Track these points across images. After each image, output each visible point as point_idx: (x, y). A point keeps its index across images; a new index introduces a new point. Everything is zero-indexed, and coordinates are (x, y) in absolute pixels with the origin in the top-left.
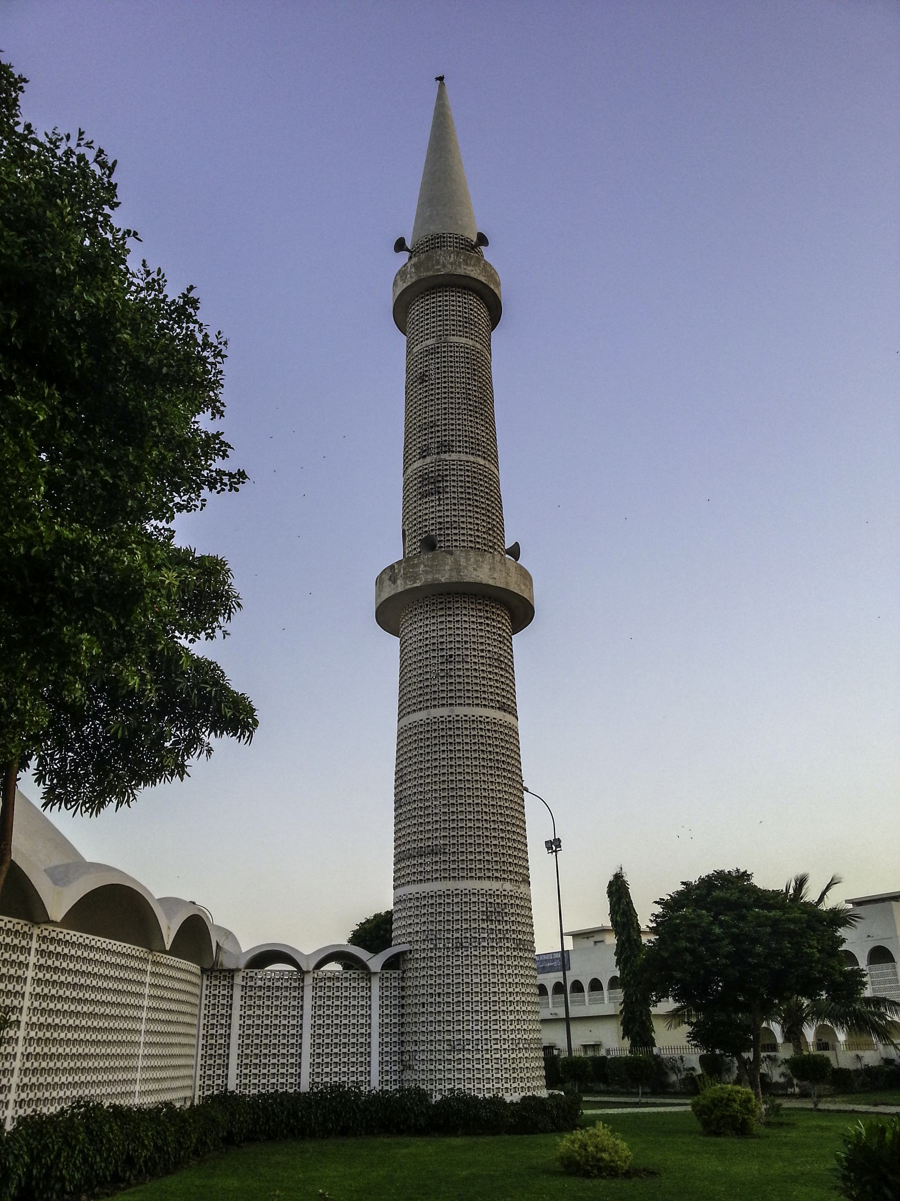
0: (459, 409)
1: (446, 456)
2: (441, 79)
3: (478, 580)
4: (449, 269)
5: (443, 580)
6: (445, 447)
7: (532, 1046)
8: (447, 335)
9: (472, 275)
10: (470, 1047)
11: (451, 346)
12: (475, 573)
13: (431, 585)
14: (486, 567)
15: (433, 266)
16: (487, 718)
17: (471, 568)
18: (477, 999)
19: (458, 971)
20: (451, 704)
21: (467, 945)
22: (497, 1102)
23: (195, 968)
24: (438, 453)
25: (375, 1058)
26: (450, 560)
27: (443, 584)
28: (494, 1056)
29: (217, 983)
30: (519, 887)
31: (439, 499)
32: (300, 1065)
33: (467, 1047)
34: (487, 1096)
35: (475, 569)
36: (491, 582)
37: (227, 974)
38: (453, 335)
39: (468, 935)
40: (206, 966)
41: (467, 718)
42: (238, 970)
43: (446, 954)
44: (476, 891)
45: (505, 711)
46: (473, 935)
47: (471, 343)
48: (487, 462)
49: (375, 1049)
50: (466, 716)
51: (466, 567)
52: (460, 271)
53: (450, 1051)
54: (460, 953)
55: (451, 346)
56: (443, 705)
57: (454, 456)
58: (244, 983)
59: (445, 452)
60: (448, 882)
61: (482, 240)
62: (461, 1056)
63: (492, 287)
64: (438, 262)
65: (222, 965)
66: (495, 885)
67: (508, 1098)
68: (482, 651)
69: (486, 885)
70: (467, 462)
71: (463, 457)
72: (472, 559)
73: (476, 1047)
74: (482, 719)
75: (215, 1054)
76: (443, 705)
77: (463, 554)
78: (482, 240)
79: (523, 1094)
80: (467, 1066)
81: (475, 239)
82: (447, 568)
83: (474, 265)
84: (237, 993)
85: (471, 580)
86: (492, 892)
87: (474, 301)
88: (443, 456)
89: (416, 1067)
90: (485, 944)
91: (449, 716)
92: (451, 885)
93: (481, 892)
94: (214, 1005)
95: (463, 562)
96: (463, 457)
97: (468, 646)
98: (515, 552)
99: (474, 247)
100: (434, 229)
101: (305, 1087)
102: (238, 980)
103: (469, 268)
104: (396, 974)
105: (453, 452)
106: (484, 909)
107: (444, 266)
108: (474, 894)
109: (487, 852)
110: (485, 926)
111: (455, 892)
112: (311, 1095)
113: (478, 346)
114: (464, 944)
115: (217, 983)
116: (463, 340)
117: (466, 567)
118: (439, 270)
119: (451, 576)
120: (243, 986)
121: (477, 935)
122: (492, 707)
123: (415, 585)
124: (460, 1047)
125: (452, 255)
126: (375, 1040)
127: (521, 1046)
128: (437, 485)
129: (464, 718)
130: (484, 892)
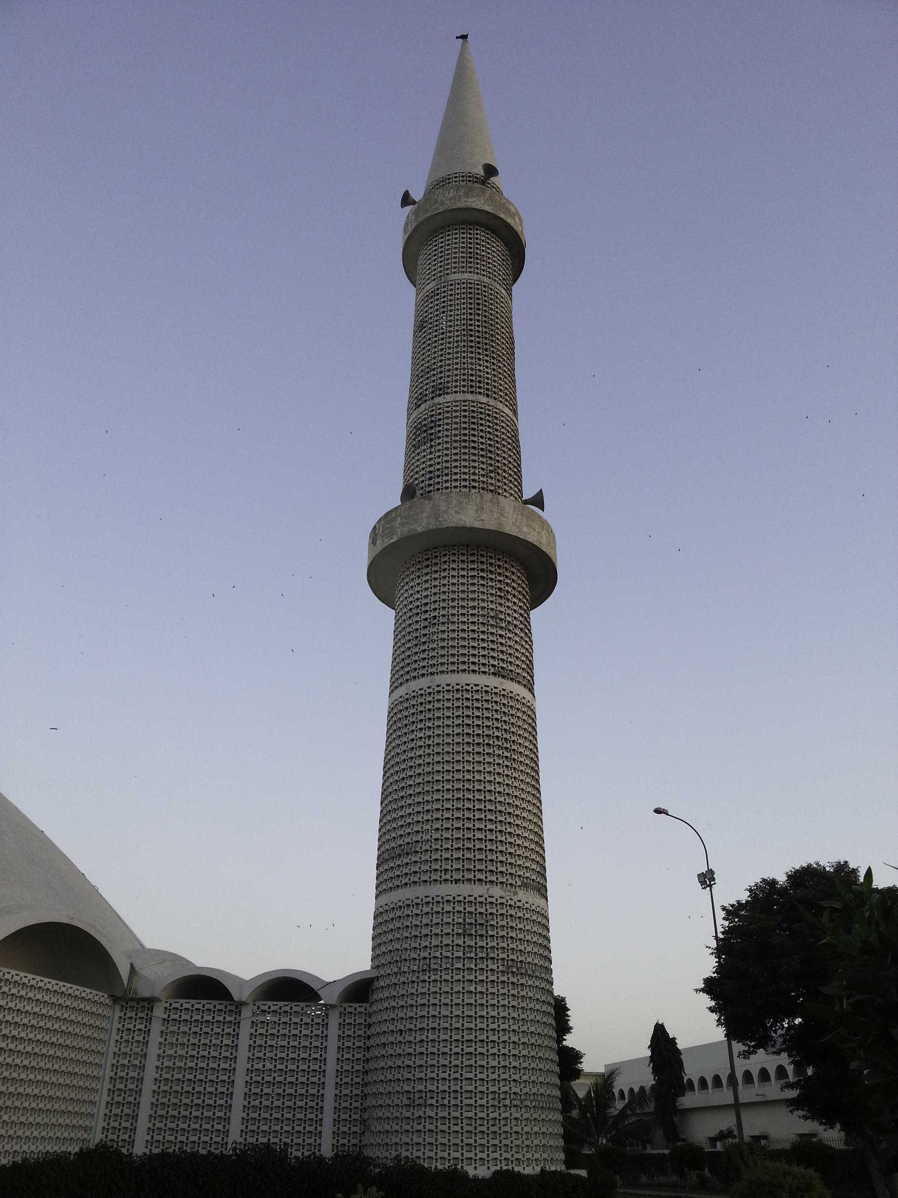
0: (457, 347)
1: (440, 400)
2: (464, 37)
3: (461, 524)
4: (449, 205)
5: (419, 530)
6: (440, 390)
7: (528, 1103)
8: (447, 274)
9: (474, 206)
10: (434, 1102)
11: (451, 285)
12: (457, 516)
13: (408, 537)
14: (471, 510)
15: (431, 206)
16: (476, 685)
17: (452, 512)
18: (457, 1037)
19: (423, 1001)
20: (432, 674)
21: (436, 967)
22: (455, 1177)
23: (102, 997)
24: (433, 398)
25: (328, 1116)
26: (428, 506)
27: (421, 534)
28: (465, 1114)
29: (133, 1015)
30: (516, 893)
31: (431, 446)
32: (228, 1120)
33: (429, 1102)
34: (440, 1167)
35: (457, 512)
36: (477, 525)
37: (145, 1004)
38: (455, 273)
39: (438, 954)
40: (119, 994)
41: (450, 688)
42: (158, 1000)
43: (410, 979)
44: (451, 898)
45: (503, 677)
46: (445, 954)
47: (476, 277)
48: (498, 403)
49: (329, 1104)
50: (448, 685)
51: (446, 512)
52: (459, 205)
53: (409, 1105)
54: (426, 978)
55: (451, 285)
56: (423, 675)
57: (449, 398)
58: (166, 1016)
59: (440, 395)
60: (428, 887)
61: (491, 171)
62: (421, 1113)
63: (502, 216)
64: (436, 202)
65: (135, 992)
66: (478, 890)
67: (471, 1172)
68: (474, 608)
69: (465, 890)
70: (464, 401)
71: (460, 397)
72: (454, 502)
73: (440, 1102)
74: (469, 688)
75: (124, 1101)
76: (423, 675)
77: (443, 497)
78: (491, 171)
79: (493, 1169)
80: (428, 1127)
81: (482, 172)
82: (425, 515)
83: (478, 196)
84: (156, 1027)
85: (451, 525)
86: (472, 899)
87: (481, 235)
88: (437, 400)
89: (373, 1128)
90: (460, 965)
91: (429, 688)
92: (420, 891)
93: (458, 899)
94: (127, 1041)
95: (443, 506)
96: (460, 397)
97: (455, 604)
98: (538, 501)
99: (484, 182)
100: (444, 173)
101: (139, 1149)
102: (159, 1012)
103: (470, 200)
104: (360, 1007)
105: (447, 393)
106: (461, 920)
107: (442, 203)
108: (448, 901)
109: (501, 852)
110: (460, 942)
111: (425, 900)
112: (150, 1158)
113: (486, 280)
114: (432, 966)
115: (133, 1015)
116: (466, 276)
117: (446, 512)
118: (437, 209)
119: (428, 524)
120: (164, 1019)
121: (449, 954)
122: (484, 672)
123: (392, 541)
124: (421, 1101)
125: (451, 191)
126: (330, 1092)
127: (508, 1102)
128: (429, 432)
129: (446, 688)
130: (461, 898)
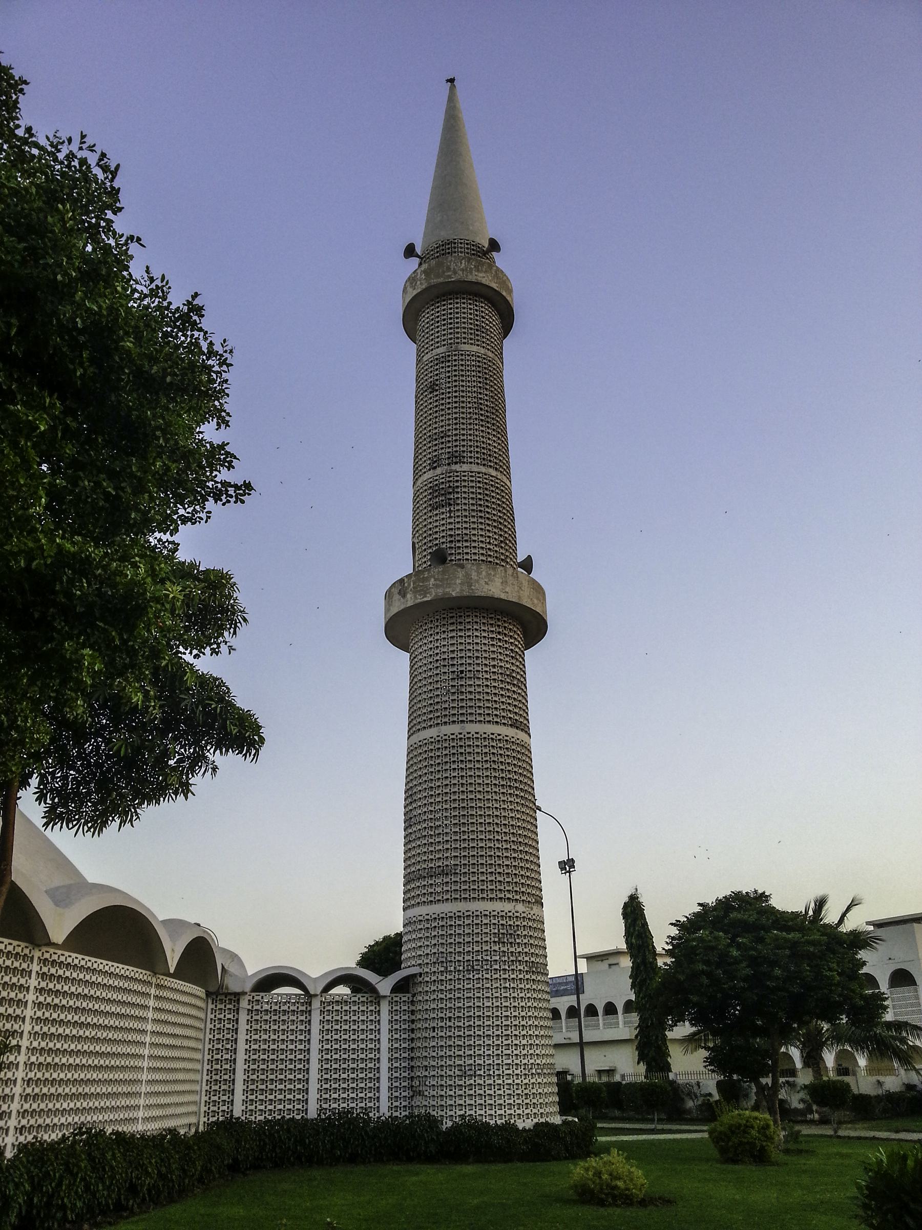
0: (470, 418)
1: (456, 467)
2: (451, 81)
3: (490, 594)
4: (460, 276)
5: (454, 594)
6: (456, 458)
7: (545, 1071)
8: (458, 343)
9: (484, 281)
10: (482, 1072)
11: (462, 355)
12: (486, 586)
13: (442, 599)
14: (498, 581)
15: (444, 272)
16: (499, 735)
17: (482, 582)
18: (488, 1023)
19: (469, 995)
20: (462, 721)
21: (479, 967)
22: (509, 1128)
23: (200, 991)
24: (449, 464)
25: (384, 1084)
26: (461, 573)
27: (454, 598)
28: (506, 1082)
29: (222, 1006)
30: (532, 909)
31: (450, 511)
32: (307, 1091)
33: (478, 1073)
34: (499, 1122)
35: (486, 583)
36: (503, 596)
37: (232, 997)
38: (465, 343)
39: (479, 958)
40: (211, 989)
41: (478, 736)
42: (244, 993)
43: (457, 977)
44: (488, 913)
45: (517, 728)
46: (485, 958)
47: (483, 351)
48: (499, 474)
49: (384, 1075)
50: (477, 733)
51: (477, 581)
52: (471, 278)
53: (461, 1076)
54: (471, 976)
55: (462, 355)
56: (454, 722)
57: (465, 467)
58: (250, 1007)
59: (456, 463)
60: (459, 903)
61: (494, 245)
62: (472, 1082)
63: (504, 294)
64: (449, 269)
65: (227, 988)
66: (507, 907)
67: (520, 1125)
68: (494, 666)
69: (498, 906)
70: (479, 473)
71: (475, 468)
72: (484, 573)
73: (487, 1073)
74: (494, 737)
75: (220, 1079)
76: (454, 722)
77: (475, 568)
78: (494, 245)
79: (536, 1121)
80: (478, 1092)
81: (486, 245)
82: (458, 581)
83: (486, 272)
84: (243, 1017)
85: (483, 594)
86: (504, 914)
87: (485, 309)
88: (454, 467)
89: (426, 1093)
90: (497, 967)
91: (460, 734)
92: (462, 906)
93: (493, 913)
94: (219, 1029)
95: (474, 575)
96: (475, 468)
97: (479, 661)
98: (527, 565)
99: (485, 253)
100: (445, 234)
101: (312, 1114)
102: (244, 1004)
103: (481, 275)
104: (405, 997)
105: (464, 463)
106: (496, 931)
107: (455, 272)
108: (486, 915)
109: (499, 873)
110: (497, 948)
111: (466, 914)
112: (318, 1122)
113: (490, 354)
114: (475, 967)
115: (222, 1006)
116: (475, 348)
117: (477, 581)
118: (450, 277)
119: (462, 590)
120: (249, 1010)
121: (488, 958)
122: (504, 724)
123: (425, 599)
124: (472, 1073)
125: (463, 262)
126: (384, 1065)
127: (534, 1071)
128: (448, 497)
129: (476, 736)
130: (495, 913)
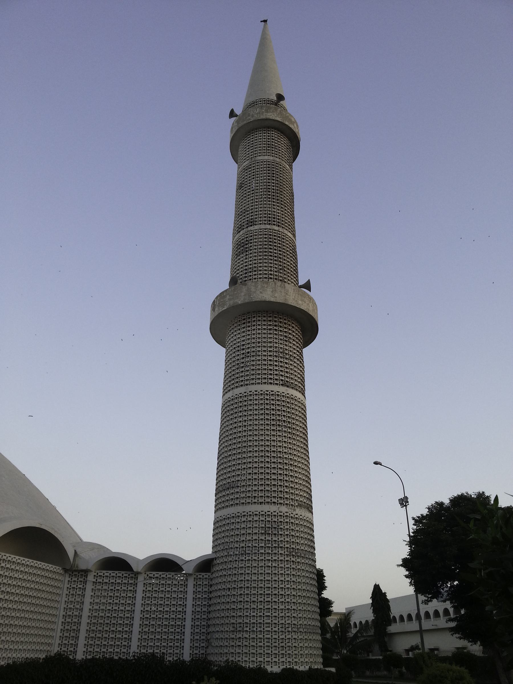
0: (261, 198)
1: (251, 228)
2: (265, 21)
3: (263, 299)
4: (256, 117)
5: (240, 302)
6: (251, 223)
7: (302, 630)
8: (256, 157)
9: (271, 117)
10: (248, 629)
11: (258, 163)
12: (261, 295)
13: (233, 307)
14: (269, 291)
15: (246, 118)
16: (272, 391)
17: (258, 292)
18: (261, 592)
19: (241, 572)
20: (247, 385)
21: (249, 552)
22: (260, 672)
23: (58, 569)
24: (247, 227)
25: (188, 637)
26: (244, 289)
27: (241, 305)
28: (266, 636)
29: (76, 579)
30: (295, 510)
31: (246, 255)
32: (130, 639)
33: (245, 629)
34: (251, 666)
35: (261, 293)
36: (272, 300)
37: (83, 573)
38: (260, 156)
39: (250, 545)
40: (68, 568)
41: (257, 393)
42: (90, 571)
43: (234, 559)
44: (258, 513)
45: (288, 386)
46: (254, 545)
47: (272, 158)
48: (285, 230)
49: (188, 630)
50: (256, 391)
51: (255, 292)
52: (262, 117)
53: (234, 631)
54: (243, 558)
55: (258, 163)
56: (242, 385)
57: (256, 227)
58: (95, 580)
59: (251, 226)
60: (245, 506)
61: (280, 97)
62: (240, 636)
63: (287, 123)
64: (249, 115)
65: (77, 567)
66: (273, 508)
67: (269, 669)
68: (271, 347)
69: (266, 508)
70: (265, 229)
71: (263, 226)
72: (259, 287)
73: (252, 629)
74: (268, 393)
75: (71, 629)
76: (242, 385)
77: (253, 284)
78: (280, 97)
79: (282, 667)
80: (245, 643)
81: (275, 98)
82: (243, 294)
83: (273, 112)
84: (89, 587)
85: (258, 300)
86: (270, 513)
87: (275, 134)
88: (249, 228)
89: (213, 644)
90: (263, 551)
91: (245, 393)
92: (240, 509)
93: (261, 513)
94: (73, 594)
95: (253, 289)
96: (263, 226)
97: (260, 345)
98: (307, 286)
99: (276, 104)
100: (253, 99)
101: (80, 656)
102: (91, 578)
103: (268, 114)
104: (206, 575)
105: (256, 225)
106: (263, 526)
107: (253, 116)
108: (256, 515)
110: (263, 538)
111: (243, 514)
112: (85, 661)
113: (278, 160)
114: (247, 552)
115: (76, 579)
116: (266, 157)
117: (255, 292)
118: (250, 119)
119: (244, 299)
120: (94, 582)
121: (257, 545)
122: (277, 384)
123: (224, 309)
124: (240, 629)
125: (258, 109)
126: (188, 623)
127: (290, 629)
128: (245, 247)
129: (255, 393)
130: (263, 513)
